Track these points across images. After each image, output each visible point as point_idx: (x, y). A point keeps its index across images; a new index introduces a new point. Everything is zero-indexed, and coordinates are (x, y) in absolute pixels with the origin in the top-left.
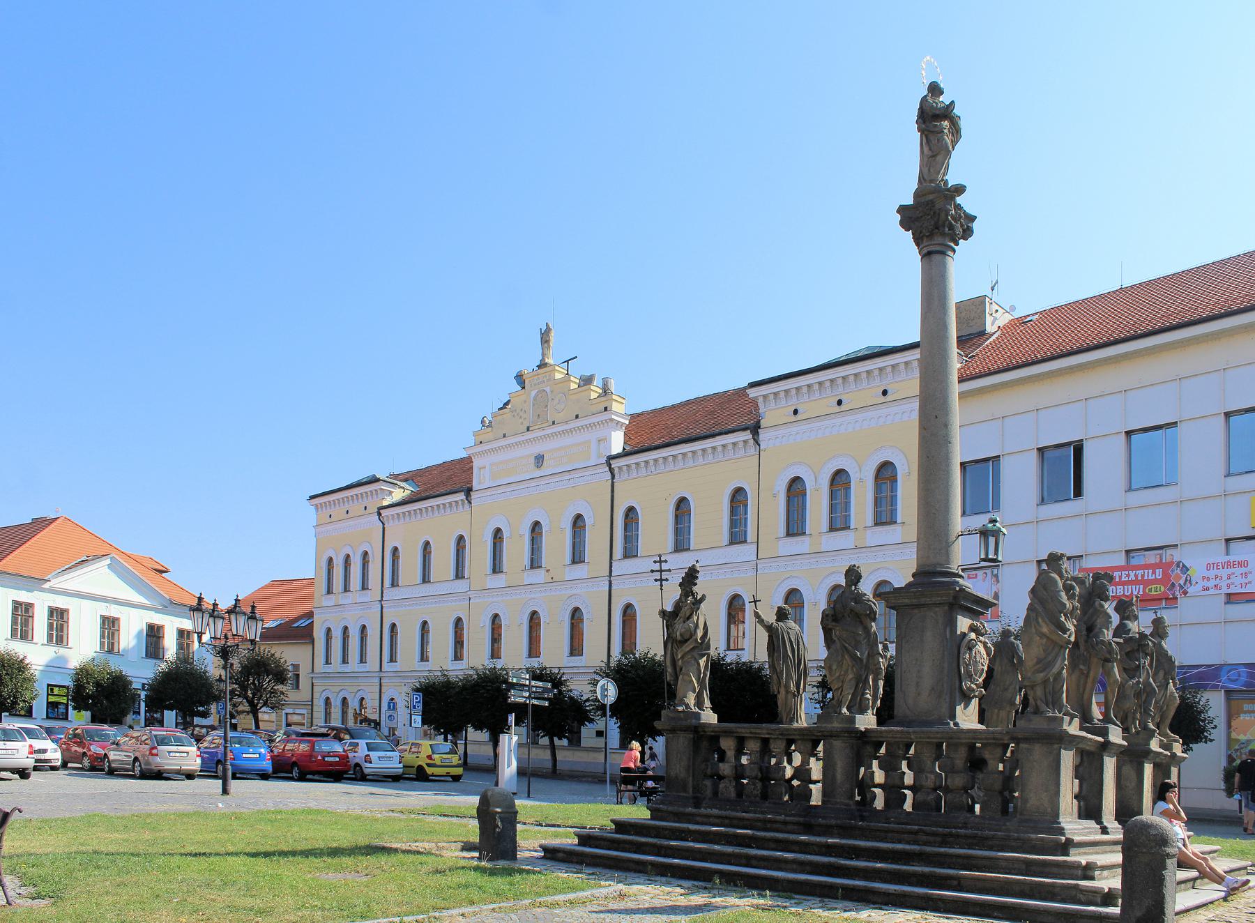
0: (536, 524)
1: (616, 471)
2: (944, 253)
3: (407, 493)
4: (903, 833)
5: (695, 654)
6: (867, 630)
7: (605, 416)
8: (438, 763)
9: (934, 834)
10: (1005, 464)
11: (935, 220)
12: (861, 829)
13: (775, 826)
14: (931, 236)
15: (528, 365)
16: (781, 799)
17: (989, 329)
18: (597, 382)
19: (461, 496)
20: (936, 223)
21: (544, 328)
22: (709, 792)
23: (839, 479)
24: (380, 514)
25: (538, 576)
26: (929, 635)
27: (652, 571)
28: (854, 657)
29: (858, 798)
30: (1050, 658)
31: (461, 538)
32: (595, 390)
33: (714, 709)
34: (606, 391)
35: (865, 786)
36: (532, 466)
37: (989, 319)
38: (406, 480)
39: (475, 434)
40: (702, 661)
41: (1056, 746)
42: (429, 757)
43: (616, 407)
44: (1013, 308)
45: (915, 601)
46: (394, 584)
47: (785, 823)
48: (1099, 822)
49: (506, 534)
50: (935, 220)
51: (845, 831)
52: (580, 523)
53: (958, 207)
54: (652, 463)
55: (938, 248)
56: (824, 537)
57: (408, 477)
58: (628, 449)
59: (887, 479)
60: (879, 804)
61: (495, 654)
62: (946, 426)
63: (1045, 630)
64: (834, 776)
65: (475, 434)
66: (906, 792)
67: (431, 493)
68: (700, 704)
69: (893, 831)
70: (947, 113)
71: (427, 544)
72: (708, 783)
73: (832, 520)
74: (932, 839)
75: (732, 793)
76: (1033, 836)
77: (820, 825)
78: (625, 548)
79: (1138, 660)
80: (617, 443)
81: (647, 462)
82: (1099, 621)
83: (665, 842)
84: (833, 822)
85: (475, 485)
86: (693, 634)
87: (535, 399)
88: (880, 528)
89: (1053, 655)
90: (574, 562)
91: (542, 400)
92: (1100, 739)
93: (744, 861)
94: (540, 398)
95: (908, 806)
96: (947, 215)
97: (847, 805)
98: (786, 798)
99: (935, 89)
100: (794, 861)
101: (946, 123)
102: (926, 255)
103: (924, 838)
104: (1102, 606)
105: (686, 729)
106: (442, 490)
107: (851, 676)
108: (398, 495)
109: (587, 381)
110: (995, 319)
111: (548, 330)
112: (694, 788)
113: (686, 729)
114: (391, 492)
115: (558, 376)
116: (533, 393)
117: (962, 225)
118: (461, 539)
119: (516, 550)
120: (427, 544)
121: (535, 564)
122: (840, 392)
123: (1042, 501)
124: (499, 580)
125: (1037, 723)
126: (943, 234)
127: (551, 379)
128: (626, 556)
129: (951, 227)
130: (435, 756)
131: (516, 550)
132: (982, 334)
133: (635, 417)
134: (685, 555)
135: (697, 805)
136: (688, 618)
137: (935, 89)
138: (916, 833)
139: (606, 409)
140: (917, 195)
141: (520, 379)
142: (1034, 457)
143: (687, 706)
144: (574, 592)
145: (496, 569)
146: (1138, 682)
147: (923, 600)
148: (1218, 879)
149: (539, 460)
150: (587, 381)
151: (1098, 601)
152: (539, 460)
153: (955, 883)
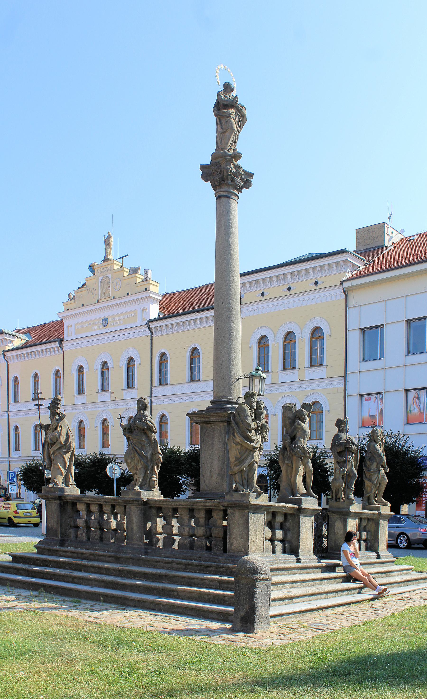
0: (105, 363)
1: (153, 330)
2: (229, 197)
3: (24, 341)
4: (165, 563)
5: (61, 451)
6: (149, 438)
7: (146, 294)
8: (22, 515)
9: (181, 564)
10: (387, 329)
11: (224, 176)
12: (143, 560)
13: (100, 558)
14: (220, 185)
15: (97, 260)
16: (109, 541)
17: (387, 244)
18: (141, 272)
19: (56, 344)
20: (222, 177)
21: (106, 236)
22: (72, 537)
23: (289, 337)
24: (4, 355)
25: (106, 396)
26: (216, 440)
27: (44, 399)
28: (140, 455)
29: (145, 541)
30: (243, 458)
31: (57, 372)
32: (139, 278)
33: (78, 486)
34: (146, 278)
35: (151, 534)
36: (101, 326)
37: (387, 238)
38: (25, 333)
39: (64, 304)
40: (67, 457)
41: (246, 511)
42: (16, 512)
43: (152, 288)
44: (403, 231)
45: (207, 420)
46: (16, 400)
47: (105, 556)
48: (377, 552)
49: (85, 369)
50: (224, 176)
51: (136, 561)
52: (131, 363)
53: (237, 167)
54: (175, 325)
55: (225, 194)
56: (280, 374)
57: (25, 331)
58: (162, 315)
59: (318, 338)
60: (160, 545)
61: (105, 444)
62: (229, 309)
63: (238, 440)
64: (132, 528)
65: (64, 304)
66: (175, 537)
67: (36, 342)
68: (66, 482)
69: (159, 562)
70: (232, 104)
71: (36, 375)
72: (72, 531)
73: (285, 363)
74: (180, 566)
75: (85, 537)
76: (230, 565)
77: (122, 558)
78: (161, 379)
79: (346, 457)
80: (154, 311)
81: (172, 324)
82: (299, 434)
83: (101, 564)
84: (128, 556)
85: (65, 337)
86: (58, 439)
87: (101, 282)
88: (313, 369)
89: (245, 455)
90: (129, 387)
91: (106, 283)
92: (296, 506)
93: (71, 579)
94: (106, 282)
95: (176, 546)
96: (228, 172)
97: (140, 545)
98: (112, 541)
99: (228, 87)
100: (95, 580)
101: (232, 111)
102: (219, 198)
103: (175, 566)
104: (299, 425)
105: (55, 498)
106: (46, 340)
107: (140, 466)
108: (17, 343)
109: (134, 271)
110: (391, 238)
111: (109, 236)
112: (62, 534)
113: (55, 498)
114: (12, 341)
115: (116, 267)
116: (100, 278)
117: (242, 179)
118: (57, 372)
119: (92, 380)
120: (36, 375)
121: (104, 388)
122: (289, 282)
123: (409, 353)
124: (82, 399)
125: (236, 497)
126: (228, 185)
127: (112, 269)
128: (161, 384)
129: (233, 180)
130: (20, 511)
131: (92, 380)
132: (383, 247)
133: (165, 296)
134: (196, 384)
135: (62, 544)
136: (56, 429)
137: (228, 87)
138: (172, 562)
139: (146, 290)
140: (214, 157)
141: (91, 268)
142: (403, 326)
143: (56, 484)
144: (129, 406)
145: (80, 391)
146: (344, 470)
147: (212, 419)
148: (374, 587)
149: (105, 322)
150: (134, 271)
151: (298, 421)
152: (105, 322)
153: (176, 594)
